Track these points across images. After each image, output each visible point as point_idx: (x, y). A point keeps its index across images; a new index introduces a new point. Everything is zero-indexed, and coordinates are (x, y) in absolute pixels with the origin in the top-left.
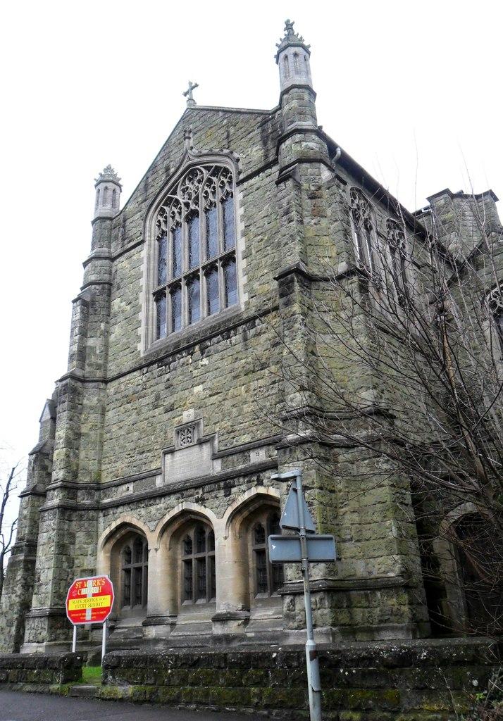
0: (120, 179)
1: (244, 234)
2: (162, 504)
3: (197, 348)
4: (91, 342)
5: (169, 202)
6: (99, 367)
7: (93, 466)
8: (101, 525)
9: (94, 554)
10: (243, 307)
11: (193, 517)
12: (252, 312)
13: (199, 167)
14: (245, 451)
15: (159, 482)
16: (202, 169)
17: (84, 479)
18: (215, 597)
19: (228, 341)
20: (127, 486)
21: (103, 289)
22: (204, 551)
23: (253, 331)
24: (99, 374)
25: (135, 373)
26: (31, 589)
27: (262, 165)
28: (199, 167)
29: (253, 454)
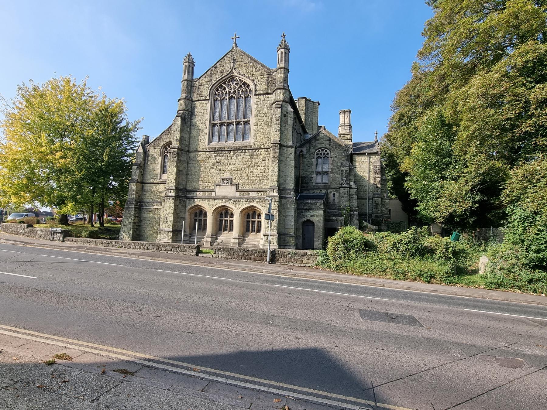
0: (195, 62)
1: (256, 116)
2: (216, 201)
3: (232, 152)
4: (184, 135)
5: (221, 86)
6: (186, 145)
7: (184, 183)
8: (187, 204)
9: (185, 213)
10: (252, 144)
11: (226, 207)
12: (256, 146)
13: (237, 78)
14: (248, 191)
15: (213, 194)
16: (238, 80)
17: (181, 187)
18: (206, 230)
19: (245, 153)
20: (200, 192)
21: (189, 113)
22: (249, 218)
23: (255, 153)
24: (187, 149)
25: (203, 153)
26: (374, 227)
27: (264, 92)
28: (237, 78)
29: (251, 193)
